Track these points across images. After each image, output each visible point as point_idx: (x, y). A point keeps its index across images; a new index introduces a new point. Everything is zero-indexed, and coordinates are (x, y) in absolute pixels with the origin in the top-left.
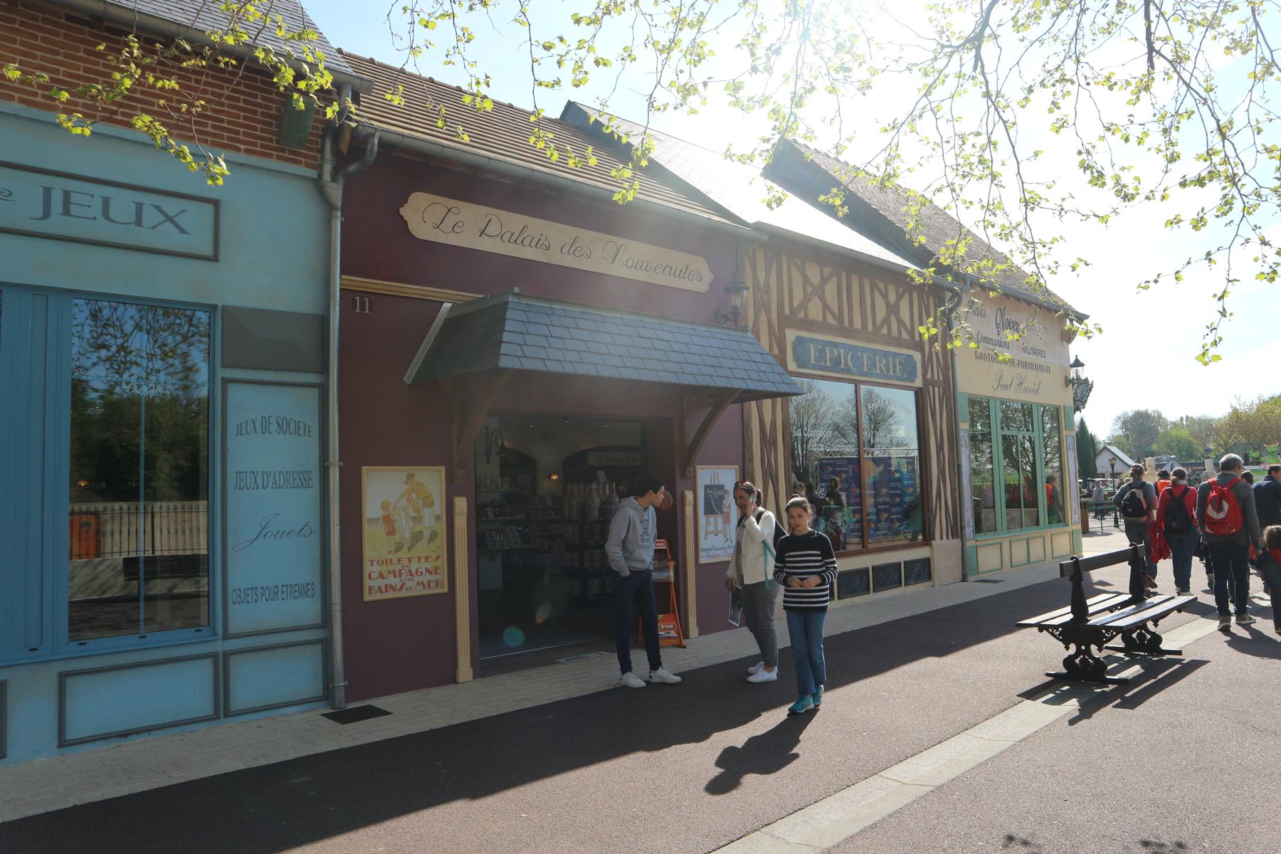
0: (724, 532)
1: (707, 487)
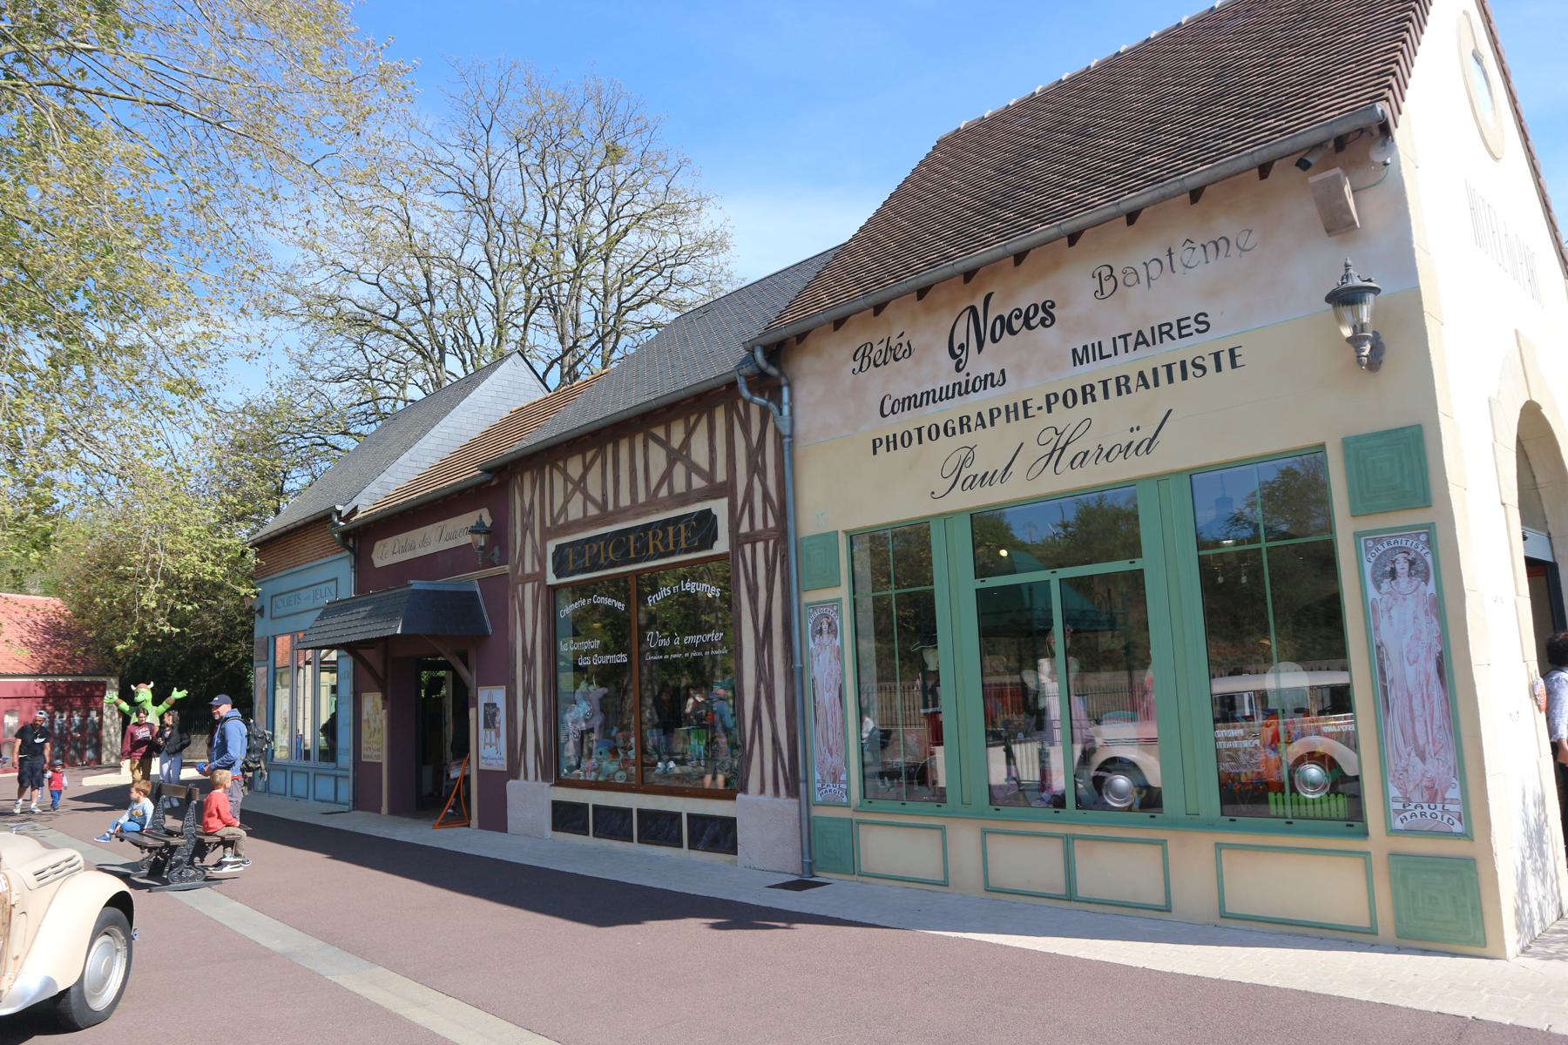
0: (496, 745)
1: (486, 705)
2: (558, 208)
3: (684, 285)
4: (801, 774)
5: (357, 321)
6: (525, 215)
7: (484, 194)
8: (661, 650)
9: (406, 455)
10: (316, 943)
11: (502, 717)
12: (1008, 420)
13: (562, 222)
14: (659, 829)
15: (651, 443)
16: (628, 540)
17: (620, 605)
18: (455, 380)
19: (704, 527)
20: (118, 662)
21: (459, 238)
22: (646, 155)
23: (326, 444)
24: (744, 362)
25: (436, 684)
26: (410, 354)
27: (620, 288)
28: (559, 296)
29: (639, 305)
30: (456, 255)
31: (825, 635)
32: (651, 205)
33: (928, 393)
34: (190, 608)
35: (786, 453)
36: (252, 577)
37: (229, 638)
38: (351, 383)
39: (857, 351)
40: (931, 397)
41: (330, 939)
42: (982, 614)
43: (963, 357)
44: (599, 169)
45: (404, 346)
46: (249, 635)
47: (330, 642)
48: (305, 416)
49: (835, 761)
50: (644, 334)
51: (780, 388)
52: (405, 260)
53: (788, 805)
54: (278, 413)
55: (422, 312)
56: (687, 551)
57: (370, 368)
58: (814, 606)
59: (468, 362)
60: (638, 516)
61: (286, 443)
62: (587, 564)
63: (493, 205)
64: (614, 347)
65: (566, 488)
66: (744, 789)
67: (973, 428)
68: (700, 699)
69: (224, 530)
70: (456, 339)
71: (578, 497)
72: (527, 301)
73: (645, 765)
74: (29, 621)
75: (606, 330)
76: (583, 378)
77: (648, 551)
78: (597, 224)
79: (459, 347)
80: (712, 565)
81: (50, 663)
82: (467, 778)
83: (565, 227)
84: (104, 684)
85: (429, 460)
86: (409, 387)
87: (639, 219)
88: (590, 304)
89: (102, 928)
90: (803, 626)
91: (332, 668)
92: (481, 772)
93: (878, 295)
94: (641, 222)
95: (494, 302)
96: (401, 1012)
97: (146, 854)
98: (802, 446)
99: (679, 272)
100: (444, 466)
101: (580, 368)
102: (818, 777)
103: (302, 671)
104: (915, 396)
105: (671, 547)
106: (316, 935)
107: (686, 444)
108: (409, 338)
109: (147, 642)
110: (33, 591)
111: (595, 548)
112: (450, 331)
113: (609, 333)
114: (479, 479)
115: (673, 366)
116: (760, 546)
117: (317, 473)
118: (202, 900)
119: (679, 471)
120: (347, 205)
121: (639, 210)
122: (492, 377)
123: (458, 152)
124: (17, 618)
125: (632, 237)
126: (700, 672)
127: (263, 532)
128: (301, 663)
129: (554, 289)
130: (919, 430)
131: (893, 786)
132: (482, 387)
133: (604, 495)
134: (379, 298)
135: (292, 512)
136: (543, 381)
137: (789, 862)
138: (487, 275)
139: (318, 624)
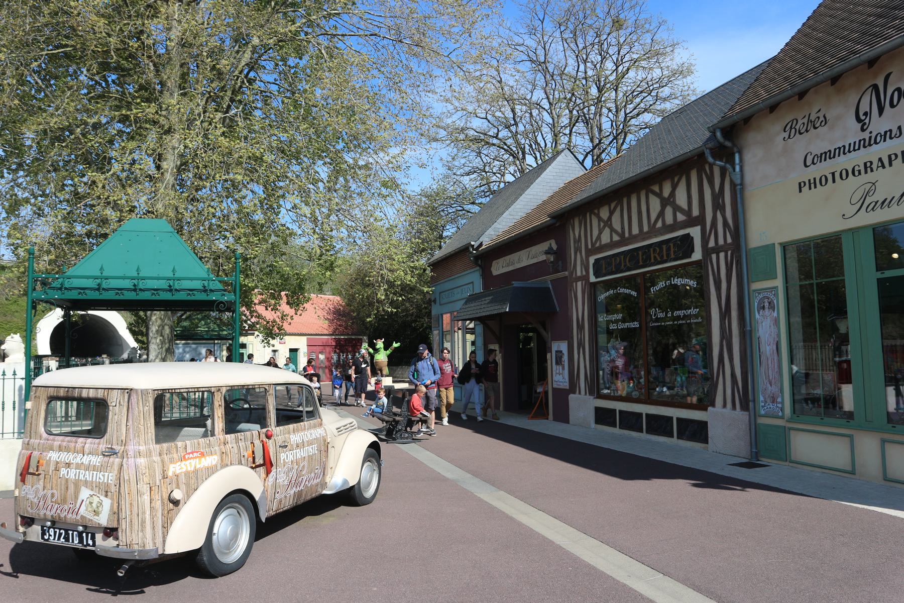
0: (562, 374)
1: (556, 352)
2: (585, 62)
3: (665, 100)
4: (751, 397)
5: (476, 140)
6: (567, 68)
7: (542, 59)
8: (657, 320)
9: (507, 213)
10: (469, 475)
11: (565, 358)
12: (810, 188)
13: (588, 70)
14: (659, 425)
15: (651, 196)
16: (638, 254)
17: (634, 293)
18: (531, 168)
19: (686, 244)
20: (367, 328)
21: (530, 87)
22: (638, 22)
23: (464, 210)
24: (708, 140)
25: (528, 340)
26: (506, 156)
27: (625, 106)
28: (589, 114)
29: (638, 115)
30: (528, 97)
31: (767, 310)
32: (642, 53)
33: (839, 148)
34: (400, 299)
35: (739, 196)
36: (430, 283)
37: (419, 316)
38: (475, 175)
39: (787, 125)
40: (842, 150)
41: (475, 474)
42: (881, 297)
43: (867, 121)
44: (609, 34)
45: (503, 152)
46: (429, 314)
47: (471, 317)
48: (452, 195)
49: (774, 389)
50: (642, 133)
51: (732, 155)
52: (500, 103)
53: (741, 416)
54: (437, 195)
55: (511, 132)
56: (675, 259)
57: (485, 166)
58: (759, 291)
59: (539, 158)
60: (644, 239)
61: (443, 211)
62: (614, 270)
63: (548, 65)
64: (624, 141)
65: (599, 225)
66: (713, 405)
67: (875, 169)
68: (681, 351)
69: (415, 257)
70: (531, 146)
71: (607, 231)
72: (571, 119)
73: (650, 387)
74: (327, 308)
75: (618, 132)
76: (605, 161)
77: (650, 260)
78: (610, 68)
79: (533, 150)
80: (690, 269)
81: (337, 329)
82: (546, 393)
83: (590, 73)
84: (361, 339)
85: (520, 214)
86: (507, 175)
87: (635, 62)
88: (607, 117)
89: (367, 458)
90: (752, 303)
91: (472, 330)
92: (554, 389)
93: (801, 85)
94: (636, 64)
95: (551, 122)
96: (514, 516)
97: (385, 424)
98: (749, 192)
99: (662, 92)
100: (528, 217)
101: (603, 156)
102: (762, 398)
103: (456, 334)
104: (830, 151)
105: (665, 258)
106: (469, 472)
107: (673, 194)
108: (505, 147)
109: (379, 318)
110: (327, 293)
111: (618, 259)
112: (527, 141)
113: (620, 133)
114: (549, 223)
115: (662, 148)
116: (722, 255)
117: (460, 226)
118: (411, 449)
119: (669, 211)
120: (468, 78)
121: (635, 56)
122: (553, 165)
123: (526, 37)
124: (321, 306)
125: (631, 74)
126: (681, 334)
127: (435, 257)
128: (456, 329)
129: (585, 110)
130: (833, 174)
131: (814, 407)
132: (548, 170)
133: (623, 228)
134: (488, 126)
135: (448, 247)
136: (582, 163)
137: (741, 448)
138: (547, 106)
139: (464, 307)
